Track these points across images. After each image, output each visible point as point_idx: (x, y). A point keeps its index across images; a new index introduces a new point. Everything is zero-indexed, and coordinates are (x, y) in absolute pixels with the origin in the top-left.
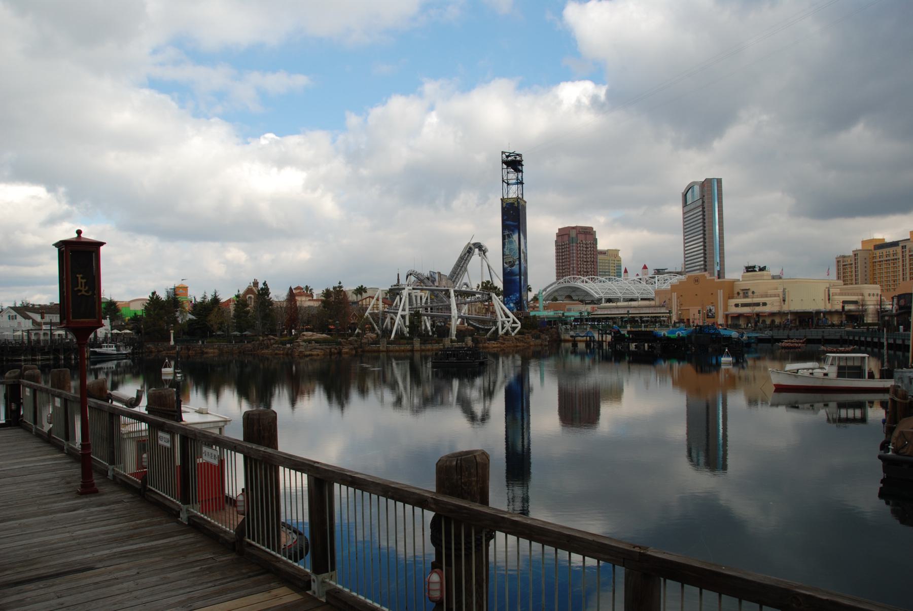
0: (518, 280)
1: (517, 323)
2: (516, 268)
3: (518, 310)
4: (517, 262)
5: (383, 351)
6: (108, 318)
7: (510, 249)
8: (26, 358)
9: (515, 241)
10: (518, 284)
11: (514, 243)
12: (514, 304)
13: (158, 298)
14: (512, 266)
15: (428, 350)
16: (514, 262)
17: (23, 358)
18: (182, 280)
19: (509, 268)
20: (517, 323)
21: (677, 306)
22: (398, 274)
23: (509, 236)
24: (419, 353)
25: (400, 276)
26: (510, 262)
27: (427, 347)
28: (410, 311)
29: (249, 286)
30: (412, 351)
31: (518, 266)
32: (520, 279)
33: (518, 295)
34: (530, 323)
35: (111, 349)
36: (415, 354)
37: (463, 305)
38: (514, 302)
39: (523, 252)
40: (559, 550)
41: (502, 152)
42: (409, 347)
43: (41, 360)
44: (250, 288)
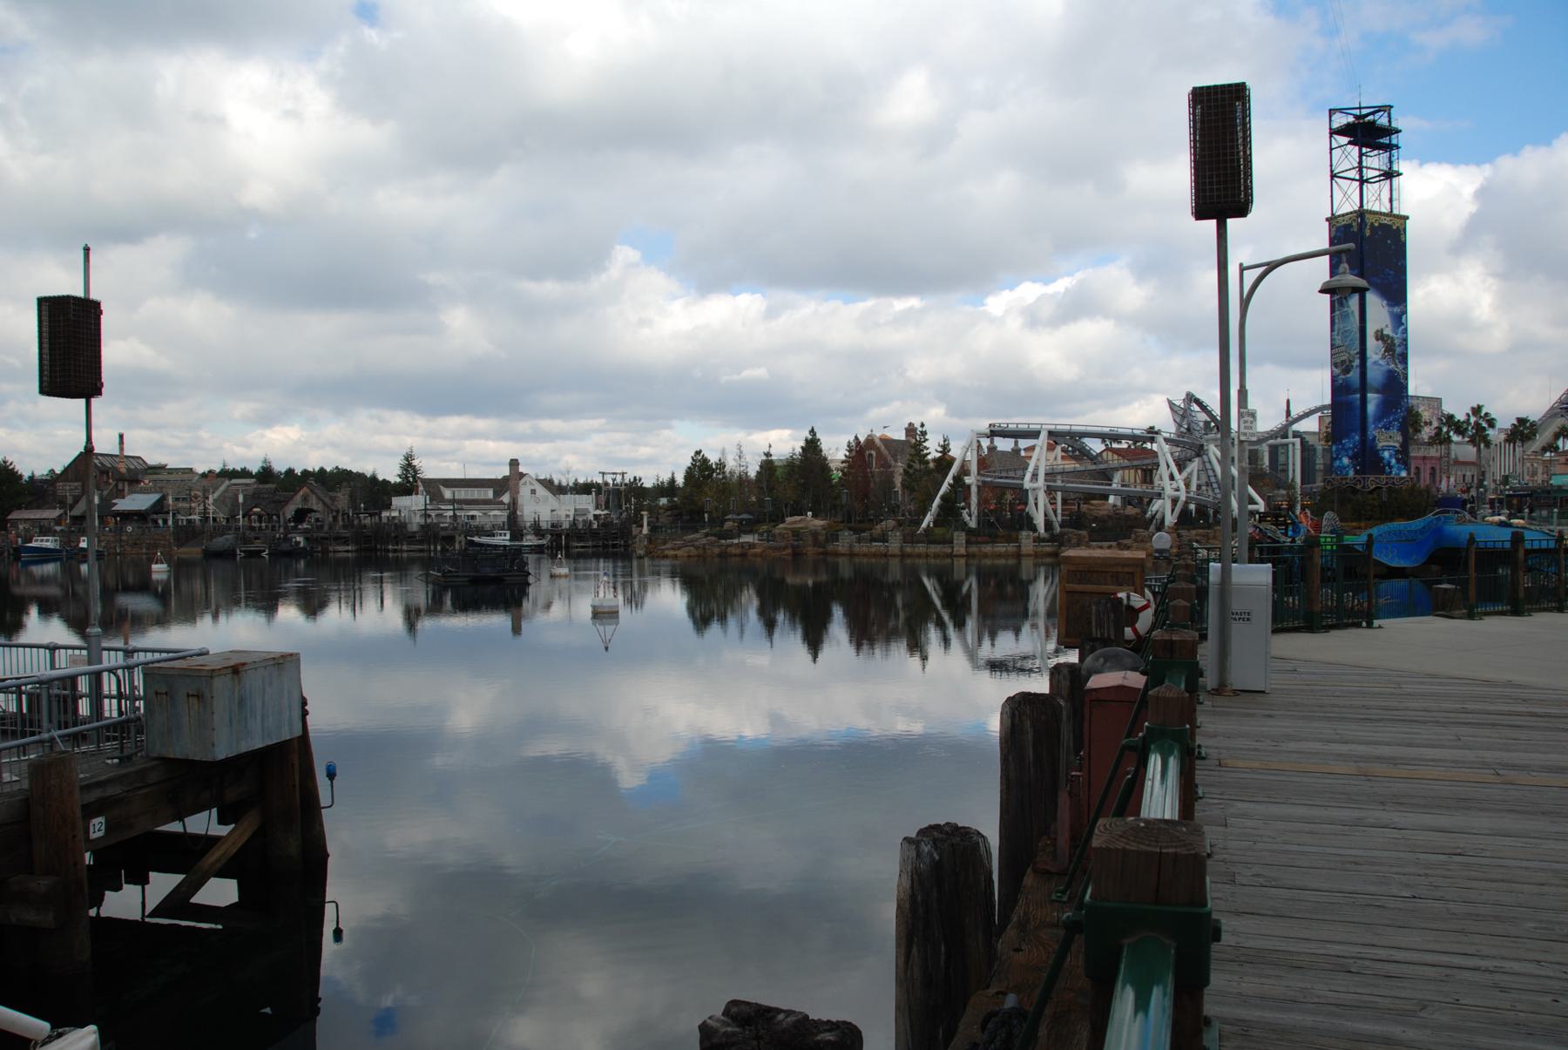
0: (1358, 402)
1: (1256, 504)
2: (1354, 375)
3: (1357, 472)
4: (1357, 362)
5: (844, 555)
6: (594, 493)
7: (1343, 333)
8: (396, 547)
9: (1353, 312)
10: (1358, 412)
11: (1352, 318)
12: (1350, 458)
13: (705, 461)
14: (1347, 370)
15: (919, 556)
16: (1350, 361)
17: (405, 547)
18: (885, 427)
19: (1342, 376)
20: (1256, 504)
21: (1210, 462)
22: (1288, 402)
23: (1341, 305)
24: (897, 560)
25: (1291, 404)
26: (1343, 362)
27: (917, 550)
28: (1046, 480)
29: (869, 436)
30: (1018, 555)
31: (1358, 370)
32: (1364, 401)
33: (1357, 438)
34: (1376, 503)
35: (503, 538)
36: (890, 562)
37: (1188, 462)
38: (1350, 453)
39: (1380, 336)
40: (182, 830)
41: (1330, 110)
42: (1011, 548)
43: (407, 551)
44: (870, 438)
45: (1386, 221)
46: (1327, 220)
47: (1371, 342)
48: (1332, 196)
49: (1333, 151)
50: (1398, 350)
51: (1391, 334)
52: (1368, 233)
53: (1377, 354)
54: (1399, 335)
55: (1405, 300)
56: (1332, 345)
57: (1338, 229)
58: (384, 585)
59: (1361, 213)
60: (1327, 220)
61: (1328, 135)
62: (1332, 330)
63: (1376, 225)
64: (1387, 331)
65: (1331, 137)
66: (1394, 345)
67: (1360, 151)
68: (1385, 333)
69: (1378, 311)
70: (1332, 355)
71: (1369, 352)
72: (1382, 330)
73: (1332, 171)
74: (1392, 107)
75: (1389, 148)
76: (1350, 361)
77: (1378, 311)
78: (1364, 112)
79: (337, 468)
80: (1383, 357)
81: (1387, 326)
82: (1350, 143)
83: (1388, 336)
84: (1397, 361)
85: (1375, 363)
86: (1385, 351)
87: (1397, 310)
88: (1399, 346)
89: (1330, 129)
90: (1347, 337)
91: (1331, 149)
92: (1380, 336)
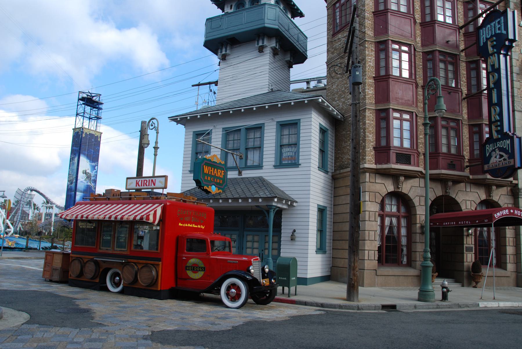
2: (73, 185)
4: (74, 181)
14: (71, 184)
19: (70, 185)
23: (73, 160)
26: (71, 180)
39: (85, 172)
45: (93, 133)
46: (73, 129)
47: (81, 175)
48: (76, 121)
49: (79, 106)
50: (92, 178)
51: (90, 172)
52: (84, 136)
53: (82, 178)
54: (93, 173)
55: (98, 161)
56: (69, 174)
57: (75, 133)
58: (417, 251)
59: (82, 128)
60: (73, 129)
61: (78, 100)
62: (69, 169)
63: (88, 133)
64: (89, 171)
65: (78, 101)
66: (91, 176)
67: (323, 78)
68: (87, 171)
69: (85, 164)
70: (68, 177)
71: (79, 178)
72: (86, 170)
73: (77, 113)
74: (100, 95)
75: (100, 109)
76: (73, 180)
77: (85, 164)
78: (93, 95)
79: (218, 8)
80: (85, 180)
81: (88, 169)
82: (83, 104)
83: (88, 173)
84: (91, 182)
85: (82, 182)
86: (86, 178)
87: (94, 164)
88: (93, 177)
89: (79, 98)
90: (73, 171)
91: (78, 105)
92: (85, 172)
